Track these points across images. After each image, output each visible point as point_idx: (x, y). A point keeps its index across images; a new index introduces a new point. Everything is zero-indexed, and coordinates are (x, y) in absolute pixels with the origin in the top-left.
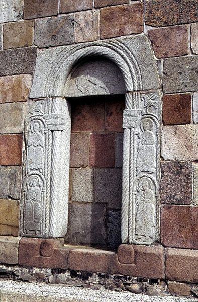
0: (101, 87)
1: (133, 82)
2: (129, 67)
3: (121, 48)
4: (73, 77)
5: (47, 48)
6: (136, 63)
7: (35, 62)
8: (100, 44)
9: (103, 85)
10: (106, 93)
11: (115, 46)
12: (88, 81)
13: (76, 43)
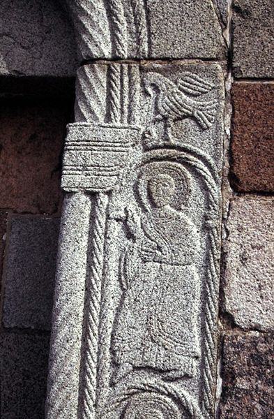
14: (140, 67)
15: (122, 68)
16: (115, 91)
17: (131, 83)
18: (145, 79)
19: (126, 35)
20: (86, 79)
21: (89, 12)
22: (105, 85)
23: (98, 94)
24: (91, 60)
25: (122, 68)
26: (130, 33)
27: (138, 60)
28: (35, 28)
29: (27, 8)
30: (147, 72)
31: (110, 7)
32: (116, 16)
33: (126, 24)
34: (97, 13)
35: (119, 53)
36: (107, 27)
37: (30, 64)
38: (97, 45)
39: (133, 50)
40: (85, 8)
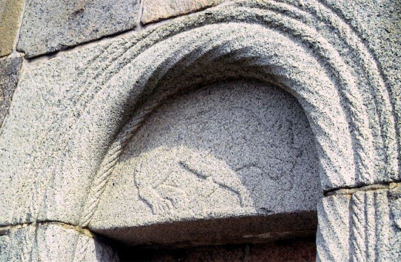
0: (223, 186)
1: (357, 146)
2: (340, 84)
3: (308, 16)
4: (126, 152)
5: (51, 54)
6: (374, 65)
7: (8, 105)
8: (227, 12)
9: (233, 179)
10: (239, 211)
11: (284, 12)
12: (179, 168)
13: (144, 25)
14: (388, 192)
15: (366, 196)
16: (357, 228)
17: (377, 215)
18: (394, 208)
19: (371, 153)
20: (325, 215)
21: (327, 131)
22: (347, 221)
23: (338, 234)
24: (330, 191)
25: (366, 196)
26: (377, 149)
27: (386, 183)
28: (284, 153)
29: (276, 129)
30: (396, 198)
31: (351, 119)
32: (358, 130)
33: (371, 138)
34: (337, 129)
35: (363, 178)
36: (350, 146)
37: (279, 198)
38: (336, 171)
39: (380, 172)
40: (323, 126)
